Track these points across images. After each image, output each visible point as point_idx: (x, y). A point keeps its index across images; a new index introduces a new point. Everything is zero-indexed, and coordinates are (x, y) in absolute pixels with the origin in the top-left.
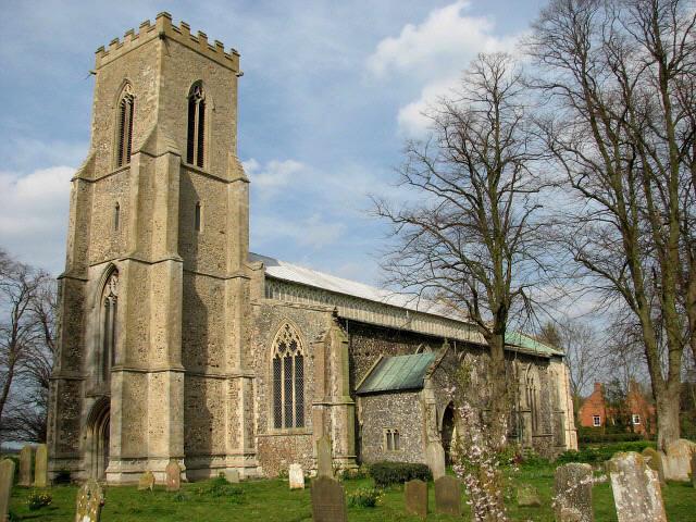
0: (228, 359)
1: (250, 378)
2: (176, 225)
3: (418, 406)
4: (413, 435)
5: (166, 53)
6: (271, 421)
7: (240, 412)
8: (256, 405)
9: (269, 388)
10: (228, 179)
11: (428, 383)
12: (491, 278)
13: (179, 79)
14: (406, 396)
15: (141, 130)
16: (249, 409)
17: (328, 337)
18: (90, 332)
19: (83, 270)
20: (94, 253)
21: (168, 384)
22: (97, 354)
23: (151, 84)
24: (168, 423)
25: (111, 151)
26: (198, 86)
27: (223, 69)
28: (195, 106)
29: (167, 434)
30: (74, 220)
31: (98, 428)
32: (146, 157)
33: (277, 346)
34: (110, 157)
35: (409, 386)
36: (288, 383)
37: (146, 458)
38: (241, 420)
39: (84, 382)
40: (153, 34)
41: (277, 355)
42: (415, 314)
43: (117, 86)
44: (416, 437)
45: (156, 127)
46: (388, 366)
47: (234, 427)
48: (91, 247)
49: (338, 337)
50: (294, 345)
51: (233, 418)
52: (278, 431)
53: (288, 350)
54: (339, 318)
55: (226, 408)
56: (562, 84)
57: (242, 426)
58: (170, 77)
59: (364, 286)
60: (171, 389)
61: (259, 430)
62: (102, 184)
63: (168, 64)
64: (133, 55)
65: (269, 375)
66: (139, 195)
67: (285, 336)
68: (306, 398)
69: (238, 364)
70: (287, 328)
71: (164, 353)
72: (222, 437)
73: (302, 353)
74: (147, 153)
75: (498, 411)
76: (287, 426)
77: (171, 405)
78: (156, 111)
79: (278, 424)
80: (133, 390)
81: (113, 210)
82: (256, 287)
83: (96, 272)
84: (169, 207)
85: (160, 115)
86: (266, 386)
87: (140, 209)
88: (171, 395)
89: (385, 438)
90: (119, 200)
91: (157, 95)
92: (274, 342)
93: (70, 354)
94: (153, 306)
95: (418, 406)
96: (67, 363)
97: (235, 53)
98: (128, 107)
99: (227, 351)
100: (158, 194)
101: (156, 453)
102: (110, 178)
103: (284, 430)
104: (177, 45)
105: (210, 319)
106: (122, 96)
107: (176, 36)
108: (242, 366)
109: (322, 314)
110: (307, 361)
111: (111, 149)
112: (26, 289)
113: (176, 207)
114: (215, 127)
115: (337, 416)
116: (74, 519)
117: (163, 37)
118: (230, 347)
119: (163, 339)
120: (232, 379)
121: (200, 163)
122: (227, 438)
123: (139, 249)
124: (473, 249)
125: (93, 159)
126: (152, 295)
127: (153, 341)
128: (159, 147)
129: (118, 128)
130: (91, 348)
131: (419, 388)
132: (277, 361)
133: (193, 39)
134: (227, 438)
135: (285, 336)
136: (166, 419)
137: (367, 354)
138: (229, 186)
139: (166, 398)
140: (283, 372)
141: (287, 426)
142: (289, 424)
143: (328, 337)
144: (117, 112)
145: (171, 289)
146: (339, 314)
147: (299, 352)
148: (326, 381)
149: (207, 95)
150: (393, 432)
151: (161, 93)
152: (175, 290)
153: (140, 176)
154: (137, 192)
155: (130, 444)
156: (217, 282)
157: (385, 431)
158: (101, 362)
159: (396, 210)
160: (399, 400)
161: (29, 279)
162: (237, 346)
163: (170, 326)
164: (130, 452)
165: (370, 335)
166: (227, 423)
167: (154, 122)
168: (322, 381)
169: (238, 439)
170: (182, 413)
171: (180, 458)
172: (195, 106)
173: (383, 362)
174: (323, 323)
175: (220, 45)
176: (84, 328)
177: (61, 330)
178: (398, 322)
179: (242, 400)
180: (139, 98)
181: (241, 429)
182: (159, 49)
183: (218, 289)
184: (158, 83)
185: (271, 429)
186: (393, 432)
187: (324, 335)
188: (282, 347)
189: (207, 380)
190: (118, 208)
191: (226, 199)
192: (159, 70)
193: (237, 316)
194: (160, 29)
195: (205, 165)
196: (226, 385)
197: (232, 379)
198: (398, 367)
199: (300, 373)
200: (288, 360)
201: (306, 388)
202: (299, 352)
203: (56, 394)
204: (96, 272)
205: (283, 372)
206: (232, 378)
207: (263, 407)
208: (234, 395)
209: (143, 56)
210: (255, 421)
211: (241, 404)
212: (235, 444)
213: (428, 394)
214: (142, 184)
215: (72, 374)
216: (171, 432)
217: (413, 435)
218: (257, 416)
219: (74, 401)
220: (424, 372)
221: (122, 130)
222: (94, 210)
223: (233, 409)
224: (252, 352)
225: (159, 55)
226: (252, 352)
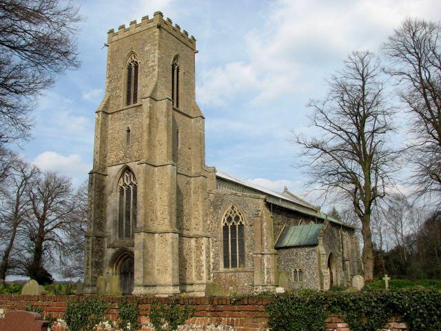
0: (194, 226)
1: (209, 238)
2: (171, 144)
3: (314, 255)
4: (311, 272)
5: (161, 37)
6: (222, 263)
7: (203, 258)
8: (212, 254)
9: (221, 244)
10: (191, 115)
11: (321, 242)
12: (363, 183)
13: (167, 54)
14: (307, 249)
15: (146, 85)
16: (208, 257)
17: (262, 213)
18: (109, 209)
19: (104, 168)
20: (111, 158)
21: (171, 240)
22: (115, 222)
23: (152, 55)
24: (171, 264)
25: (122, 95)
26: (176, 57)
27: (188, 48)
28: (175, 69)
29: (170, 270)
30: (99, 137)
31: (117, 265)
32: (153, 101)
33: (226, 219)
34: (121, 99)
35: (306, 243)
36: (233, 241)
37: (155, 286)
38: (204, 263)
39: (106, 239)
40: (151, 25)
41: (226, 224)
42: (283, 200)
43: (125, 55)
44: (313, 273)
45: (157, 83)
46: (291, 232)
47: (199, 267)
48: (109, 154)
49: (266, 214)
50: (237, 218)
51: (199, 261)
52: (226, 269)
53: (233, 221)
54: (268, 203)
55: (193, 255)
56: (431, 73)
57: (204, 266)
58: (163, 52)
59: (265, 180)
60: (172, 243)
61: (214, 269)
62: (116, 116)
63: (162, 44)
64: (137, 36)
65: (221, 236)
66: (150, 124)
67: (231, 213)
68: (247, 250)
69: (201, 229)
70: (233, 208)
71: (167, 221)
72: (191, 272)
73: (243, 223)
74: (153, 98)
75: (368, 258)
76: (232, 267)
77: (173, 253)
78: (156, 72)
79: (226, 265)
80: (149, 244)
81: (125, 133)
82: (211, 183)
83: (113, 171)
84: (168, 132)
85: (158, 75)
86: (218, 243)
87: (150, 133)
88: (173, 248)
89: (293, 274)
90: (130, 126)
91: (156, 63)
92: (224, 216)
93: (98, 221)
94: (158, 193)
95: (314, 255)
96: (96, 227)
97: (193, 38)
98: (133, 68)
99: (193, 221)
100: (160, 123)
101: (162, 282)
102: (122, 112)
103: (231, 269)
104: (166, 32)
105: (185, 201)
106: (129, 61)
107: (165, 27)
108: (203, 231)
109: (257, 200)
110: (247, 229)
111: (122, 94)
112: (26, 178)
113: (171, 133)
114: (186, 84)
115: (268, 261)
116: (322, 326)
117: (159, 27)
118: (197, 220)
119: (166, 213)
120: (197, 238)
121: (177, 106)
122: (194, 274)
123: (150, 157)
124: (354, 166)
125: (108, 101)
126: (157, 186)
127: (159, 214)
128: (159, 95)
129: (126, 81)
130: (110, 219)
131: (316, 245)
132: (225, 228)
133: (174, 29)
134: (194, 274)
135: (231, 213)
136: (170, 261)
137: (279, 224)
138: (193, 120)
139: (169, 249)
140: (230, 235)
141: (232, 267)
142: (234, 265)
143: (262, 213)
144: (124, 72)
145: (171, 182)
146: (267, 201)
147: (241, 223)
148: (262, 240)
149: (180, 63)
150: (298, 270)
151: (159, 62)
152: (173, 183)
153: (149, 112)
154: (148, 122)
155: (148, 277)
156: (189, 179)
157: (293, 270)
158: (118, 226)
159: (309, 141)
160: (302, 252)
161: (28, 173)
162: (201, 218)
163: (170, 205)
164: (147, 282)
165: (285, 212)
166: (194, 264)
167: (155, 79)
168: (259, 239)
169: (202, 274)
170: (178, 259)
171: (178, 286)
172: (175, 69)
173: (286, 229)
174: (258, 205)
175: (186, 33)
176: (105, 205)
177: (93, 206)
178: (293, 208)
179: (205, 251)
180: (142, 63)
181: (204, 268)
182: (157, 34)
183: (188, 183)
184: (157, 55)
185: (222, 268)
186: (298, 270)
187: (260, 213)
188: (229, 219)
189: (184, 238)
190: (129, 131)
191: (191, 128)
192: (157, 47)
193: (200, 200)
194: (157, 22)
195: (180, 107)
196: (193, 241)
197: (197, 238)
198: (298, 233)
199: (241, 234)
200: (233, 227)
201: (246, 244)
202: (241, 223)
203: (90, 246)
204: (113, 171)
205: (230, 235)
206: (197, 237)
207: (216, 255)
208: (199, 248)
209: (144, 37)
210: (211, 264)
211: (204, 253)
212: (201, 278)
213: (321, 248)
214: (151, 117)
215: (99, 233)
216: (173, 270)
217: (311, 272)
218: (212, 260)
219: (101, 251)
220: (316, 235)
221: (129, 87)
222: (110, 132)
223: (198, 256)
224: (209, 222)
225: (157, 38)
226: (209, 222)
